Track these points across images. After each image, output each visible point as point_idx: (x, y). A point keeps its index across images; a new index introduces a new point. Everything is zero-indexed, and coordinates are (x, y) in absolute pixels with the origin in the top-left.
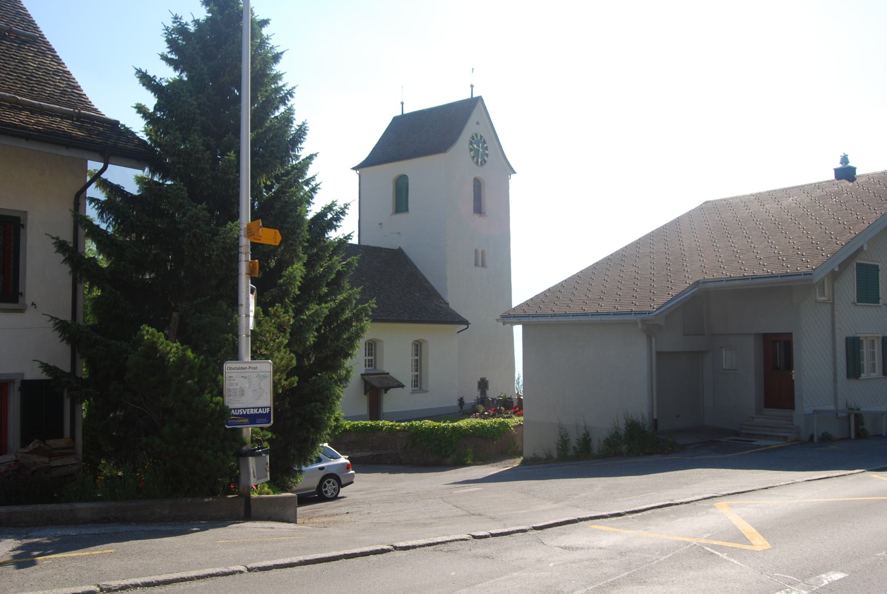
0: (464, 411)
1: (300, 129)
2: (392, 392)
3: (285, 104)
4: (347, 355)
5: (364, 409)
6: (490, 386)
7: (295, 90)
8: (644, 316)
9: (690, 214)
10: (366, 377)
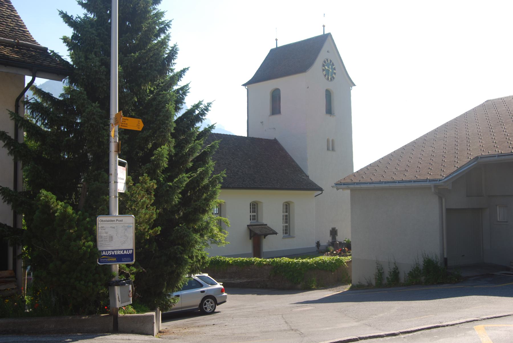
0: (320, 250)
1: (172, 50)
2: (269, 237)
3: (165, 33)
4: (204, 212)
5: (250, 249)
6: (339, 233)
7: (171, 23)
8: (436, 182)
9: (474, 110)
10: (251, 227)
